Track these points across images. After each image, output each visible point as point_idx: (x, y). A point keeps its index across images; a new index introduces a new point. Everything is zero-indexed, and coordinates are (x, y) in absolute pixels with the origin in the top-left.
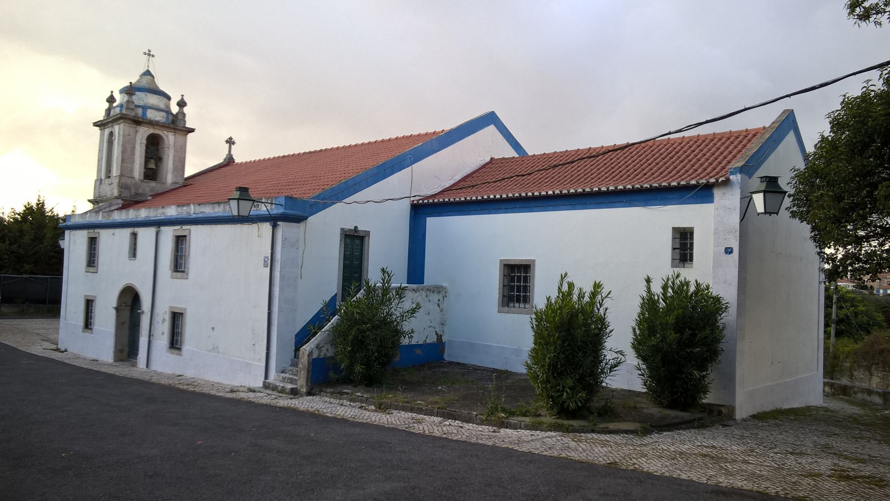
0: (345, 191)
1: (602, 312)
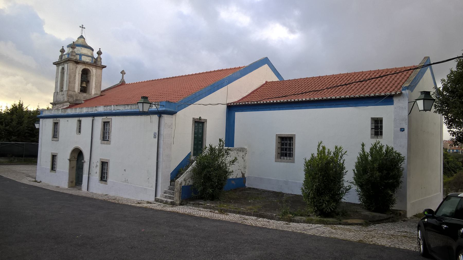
0: (195, 99)
1: (342, 162)
